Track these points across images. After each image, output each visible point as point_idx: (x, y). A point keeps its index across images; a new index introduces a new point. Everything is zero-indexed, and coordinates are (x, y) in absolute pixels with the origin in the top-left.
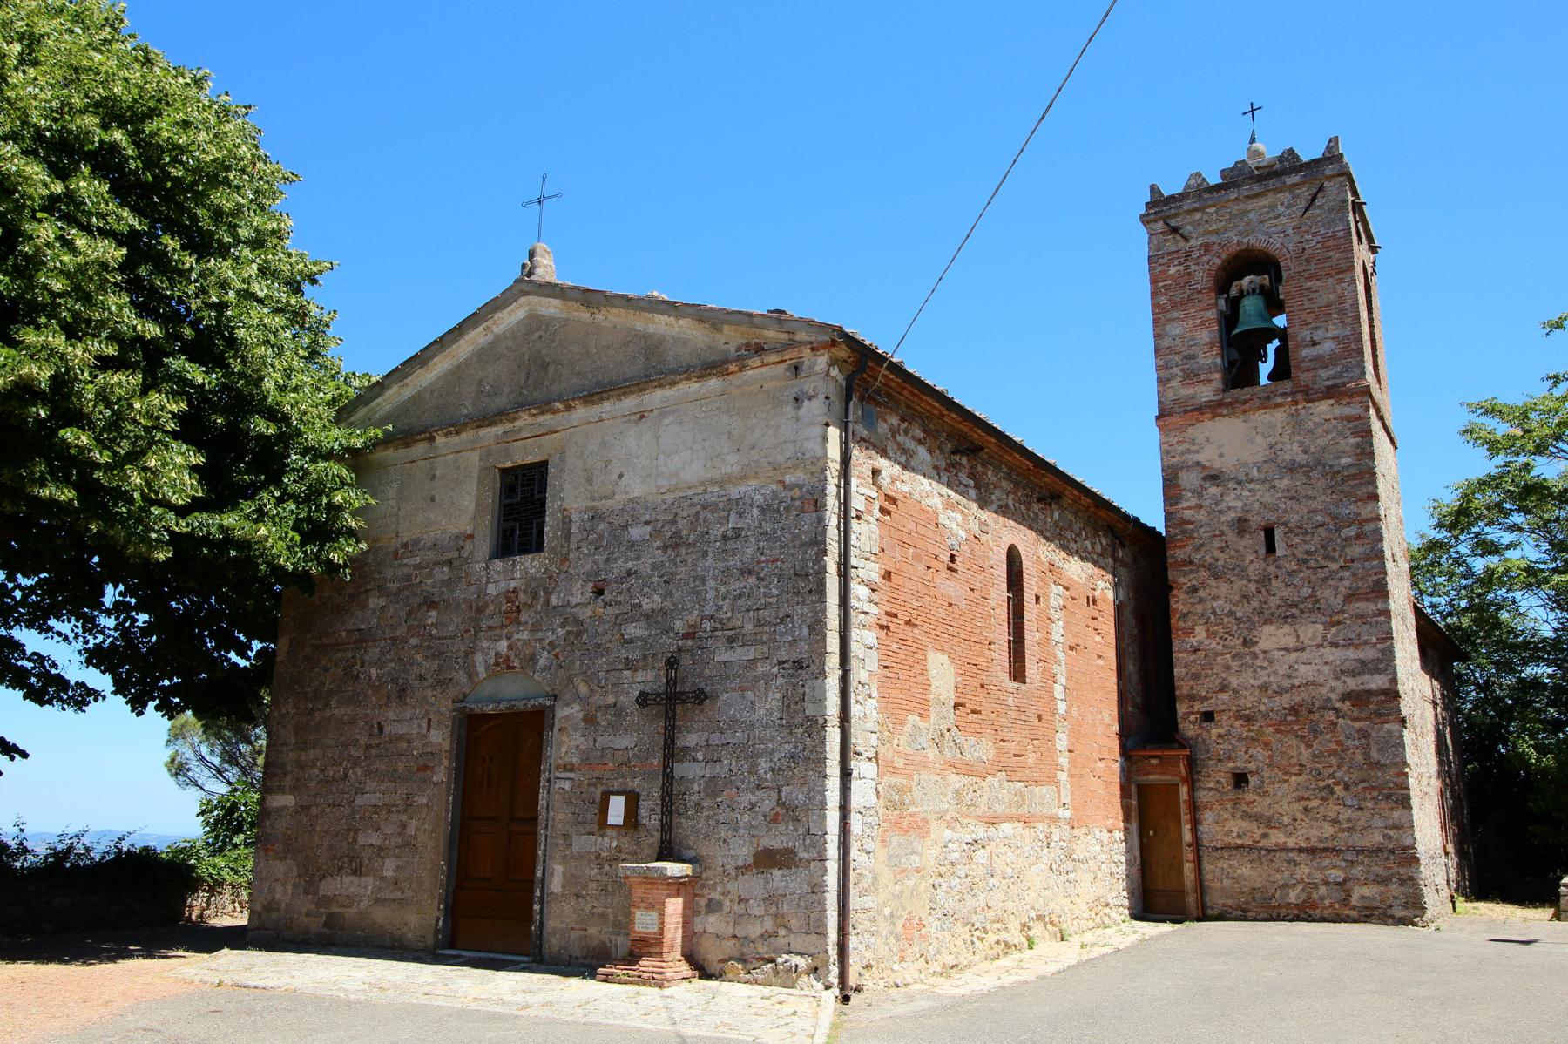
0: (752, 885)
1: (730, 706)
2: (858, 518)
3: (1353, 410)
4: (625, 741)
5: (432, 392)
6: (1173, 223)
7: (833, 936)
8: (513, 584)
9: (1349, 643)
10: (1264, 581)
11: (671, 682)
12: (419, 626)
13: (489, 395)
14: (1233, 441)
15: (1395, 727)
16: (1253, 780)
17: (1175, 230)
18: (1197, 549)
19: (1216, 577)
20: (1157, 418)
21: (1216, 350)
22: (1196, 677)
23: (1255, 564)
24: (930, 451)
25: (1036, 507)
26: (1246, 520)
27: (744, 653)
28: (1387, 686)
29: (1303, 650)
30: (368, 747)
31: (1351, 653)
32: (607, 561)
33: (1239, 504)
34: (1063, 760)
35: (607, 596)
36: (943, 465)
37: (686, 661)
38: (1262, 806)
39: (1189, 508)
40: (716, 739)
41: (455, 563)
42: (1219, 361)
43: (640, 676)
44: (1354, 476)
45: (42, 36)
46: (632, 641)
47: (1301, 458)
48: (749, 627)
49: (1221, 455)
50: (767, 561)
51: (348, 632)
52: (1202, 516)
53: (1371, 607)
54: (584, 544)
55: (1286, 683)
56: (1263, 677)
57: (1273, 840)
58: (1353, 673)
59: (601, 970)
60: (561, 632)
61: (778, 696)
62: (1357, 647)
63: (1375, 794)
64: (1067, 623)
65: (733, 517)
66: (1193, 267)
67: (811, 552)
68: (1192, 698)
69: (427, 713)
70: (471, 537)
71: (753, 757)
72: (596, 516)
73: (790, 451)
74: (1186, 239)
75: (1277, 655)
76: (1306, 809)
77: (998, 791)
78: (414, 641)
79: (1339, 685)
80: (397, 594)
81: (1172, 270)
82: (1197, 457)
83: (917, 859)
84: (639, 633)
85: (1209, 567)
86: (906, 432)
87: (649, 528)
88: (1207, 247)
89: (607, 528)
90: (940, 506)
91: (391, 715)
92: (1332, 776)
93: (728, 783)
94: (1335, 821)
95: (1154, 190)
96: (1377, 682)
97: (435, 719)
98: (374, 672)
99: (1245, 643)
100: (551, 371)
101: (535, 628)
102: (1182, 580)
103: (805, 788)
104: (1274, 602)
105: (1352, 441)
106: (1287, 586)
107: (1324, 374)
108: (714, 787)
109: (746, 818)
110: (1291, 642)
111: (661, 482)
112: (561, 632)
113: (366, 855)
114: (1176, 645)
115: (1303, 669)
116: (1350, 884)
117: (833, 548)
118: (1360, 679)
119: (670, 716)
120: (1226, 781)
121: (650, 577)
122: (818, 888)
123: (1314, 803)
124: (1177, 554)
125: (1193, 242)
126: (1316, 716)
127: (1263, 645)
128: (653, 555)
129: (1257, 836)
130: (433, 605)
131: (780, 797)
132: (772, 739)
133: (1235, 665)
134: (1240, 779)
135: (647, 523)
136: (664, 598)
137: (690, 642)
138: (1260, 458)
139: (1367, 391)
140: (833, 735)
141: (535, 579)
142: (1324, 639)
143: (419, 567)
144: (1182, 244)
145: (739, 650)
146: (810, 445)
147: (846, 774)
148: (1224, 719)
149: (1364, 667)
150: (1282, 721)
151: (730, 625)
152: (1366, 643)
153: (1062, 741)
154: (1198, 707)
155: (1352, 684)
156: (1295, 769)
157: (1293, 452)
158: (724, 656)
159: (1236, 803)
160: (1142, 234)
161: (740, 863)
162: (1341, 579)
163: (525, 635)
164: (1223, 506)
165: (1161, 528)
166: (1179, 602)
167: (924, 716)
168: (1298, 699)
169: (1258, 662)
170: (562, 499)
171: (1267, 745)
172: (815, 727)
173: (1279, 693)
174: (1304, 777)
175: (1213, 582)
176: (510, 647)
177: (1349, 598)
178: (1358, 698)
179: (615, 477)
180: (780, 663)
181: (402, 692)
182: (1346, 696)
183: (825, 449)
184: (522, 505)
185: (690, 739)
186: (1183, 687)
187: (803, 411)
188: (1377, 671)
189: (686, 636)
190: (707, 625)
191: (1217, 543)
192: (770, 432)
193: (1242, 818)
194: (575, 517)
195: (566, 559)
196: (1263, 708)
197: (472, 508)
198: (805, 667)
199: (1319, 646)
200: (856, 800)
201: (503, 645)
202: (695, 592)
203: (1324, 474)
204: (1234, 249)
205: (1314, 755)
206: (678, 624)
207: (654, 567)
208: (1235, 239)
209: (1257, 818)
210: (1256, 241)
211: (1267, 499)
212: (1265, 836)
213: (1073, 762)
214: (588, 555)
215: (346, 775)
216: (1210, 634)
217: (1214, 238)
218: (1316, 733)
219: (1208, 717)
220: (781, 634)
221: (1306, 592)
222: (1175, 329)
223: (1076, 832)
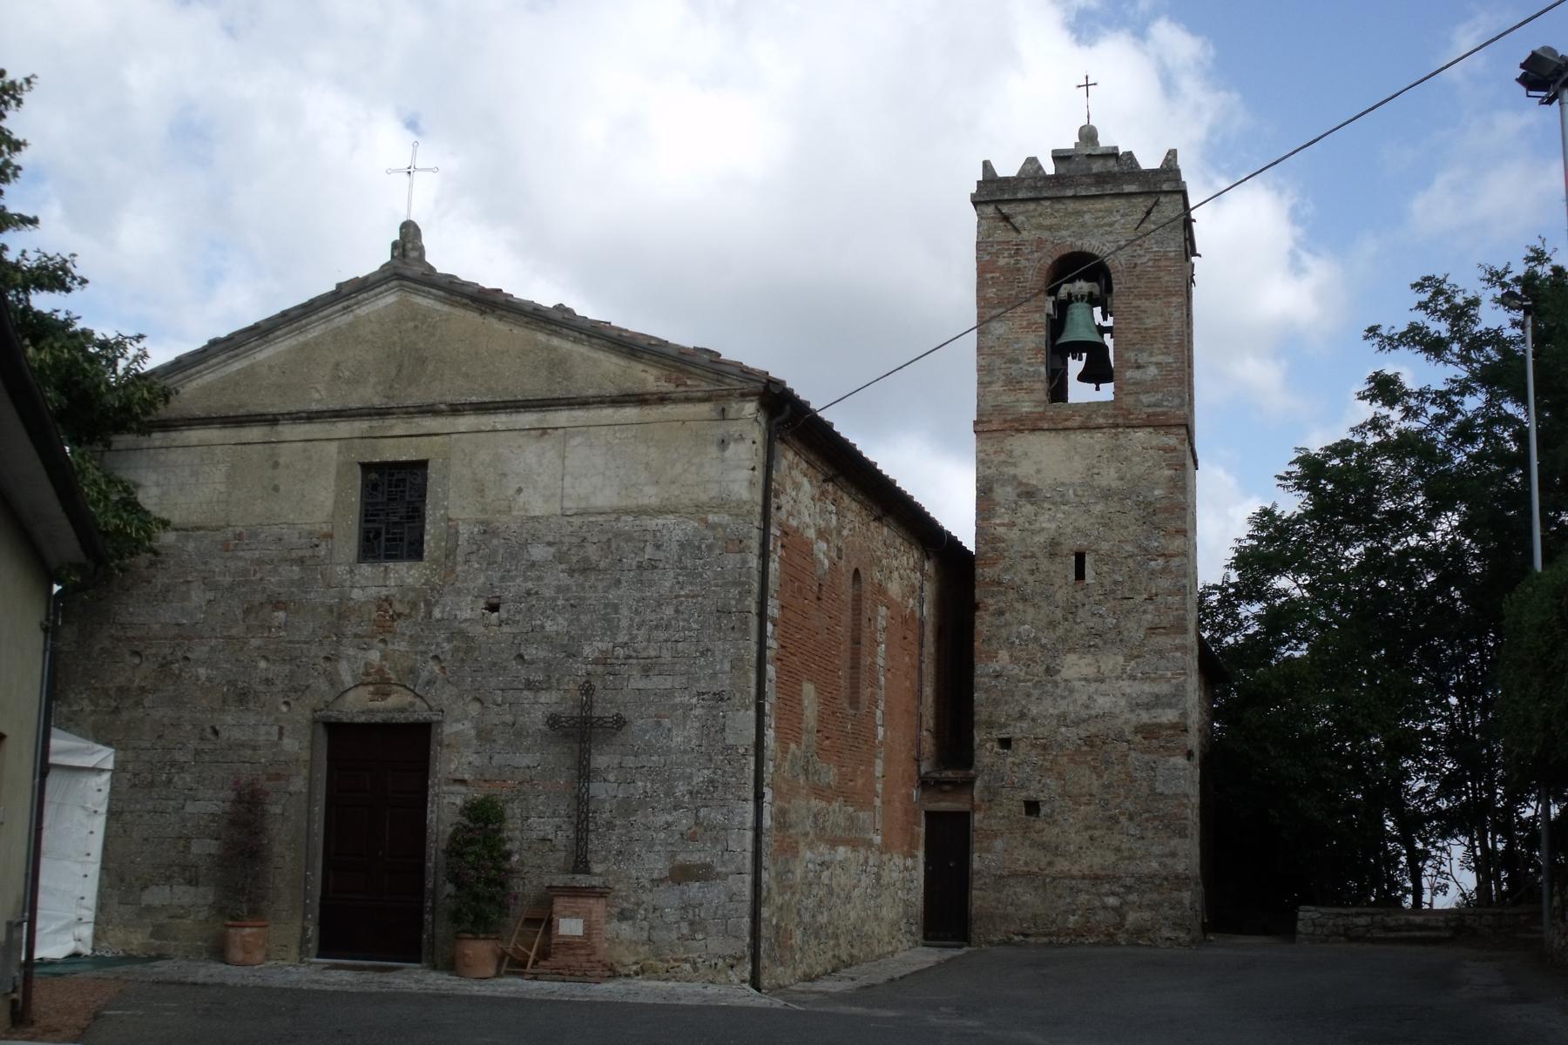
0: (668, 899)
3: (1172, 441)
4: (524, 760)
5: (271, 368)
6: (1005, 209)
8: (384, 592)
9: (1146, 677)
10: (1072, 610)
12: (262, 626)
13: (348, 382)
14: (1046, 458)
16: (1044, 810)
17: (1006, 218)
18: (1006, 570)
19: (1024, 600)
20: (976, 423)
21: (1041, 357)
22: (996, 703)
23: (1063, 592)
25: (873, 525)
26: (1058, 544)
27: (658, 682)
28: (1176, 720)
29: (1102, 681)
30: (197, 752)
31: (1147, 687)
32: (502, 579)
33: (1053, 526)
35: (503, 613)
38: (1051, 834)
40: (630, 762)
41: (309, 562)
42: (1043, 369)
43: (544, 697)
44: (1166, 510)
45: (1463, 895)
46: (532, 662)
47: (1115, 484)
48: (667, 656)
49: (1038, 471)
50: (687, 596)
51: (163, 625)
52: (1014, 534)
54: (473, 558)
55: (1084, 714)
56: (1063, 706)
57: (1058, 867)
58: (1148, 707)
61: (697, 725)
62: (1153, 680)
63: (1156, 823)
65: (649, 549)
66: (1023, 263)
68: (990, 725)
69: (277, 720)
70: (329, 536)
72: (488, 531)
73: (713, 490)
74: (1017, 230)
75: (1078, 684)
76: (1091, 838)
78: (255, 642)
79: (1133, 718)
80: (231, 588)
81: (1002, 262)
82: (1011, 471)
84: (542, 654)
85: (1017, 589)
87: (552, 550)
88: (1040, 243)
89: (499, 543)
91: (229, 719)
92: (1118, 806)
93: (642, 804)
94: (1118, 850)
97: (288, 728)
98: (202, 671)
99: (1050, 671)
100: (430, 368)
101: (414, 640)
102: (991, 601)
103: (725, 810)
104: (1081, 629)
105: (1168, 473)
107: (1145, 399)
108: (627, 808)
109: (662, 835)
110: (1090, 672)
111: (567, 504)
114: (980, 669)
115: (1101, 700)
116: (1125, 908)
118: (1154, 712)
120: (1018, 809)
121: (555, 599)
123: (1097, 833)
124: (983, 573)
125: (1025, 234)
126: (1107, 748)
127: (1065, 673)
128: (557, 576)
129: (1043, 865)
130: (278, 605)
131: (697, 817)
132: (691, 765)
133: (1036, 693)
134: (1032, 807)
135: (550, 544)
136: (571, 623)
137: (600, 669)
138: (1077, 479)
141: (413, 589)
142: (1124, 671)
143: (260, 562)
144: (1014, 234)
145: (655, 679)
148: (1022, 748)
149: (1157, 702)
150: (1078, 750)
151: (645, 654)
152: (1162, 677)
153: (879, 769)
154: (996, 734)
155: (1145, 717)
156: (1084, 799)
157: (1109, 477)
158: (638, 683)
159: (1026, 829)
160: (971, 216)
161: (655, 876)
162: (1145, 612)
163: (403, 646)
164: (1037, 526)
165: (969, 543)
166: (984, 623)
168: (1093, 730)
169: (1059, 691)
170: (446, 508)
171: (1060, 776)
173: (1076, 724)
174: (1092, 807)
175: (1019, 606)
176: (384, 657)
177: (1153, 629)
179: (511, 492)
180: (699, 694)
184: (393, 506)
185: (600, 760)
186: (981, 713)
187: (729, 453)
188: (1170, 706)
189: (596, 662)
190: (620, 652)
191: (1027, 564)
192: (693, 469)
193: (1031, 846)
194: (462, 529)
195: (453, 571)
196: (1059, 738)
197: (329, 503)
199: (1117, 678)
201: (374, 656)
202: (605, 618)
203: (1138, 504)
206: (587, 650)
207: (559, 589)
208: (1071, 241)
209: (1043, 846)
210: (1092, 244)
211: (1081, 523)
212: (1050, 864)
214: (480, 569)
215: (170, 781)
216: (1014, 659)
217: (1045, 235)
218: (1108, 763)
219: (1006, 743)
220: (701, 668)
221: (1111, 621)
222: (998, 328)
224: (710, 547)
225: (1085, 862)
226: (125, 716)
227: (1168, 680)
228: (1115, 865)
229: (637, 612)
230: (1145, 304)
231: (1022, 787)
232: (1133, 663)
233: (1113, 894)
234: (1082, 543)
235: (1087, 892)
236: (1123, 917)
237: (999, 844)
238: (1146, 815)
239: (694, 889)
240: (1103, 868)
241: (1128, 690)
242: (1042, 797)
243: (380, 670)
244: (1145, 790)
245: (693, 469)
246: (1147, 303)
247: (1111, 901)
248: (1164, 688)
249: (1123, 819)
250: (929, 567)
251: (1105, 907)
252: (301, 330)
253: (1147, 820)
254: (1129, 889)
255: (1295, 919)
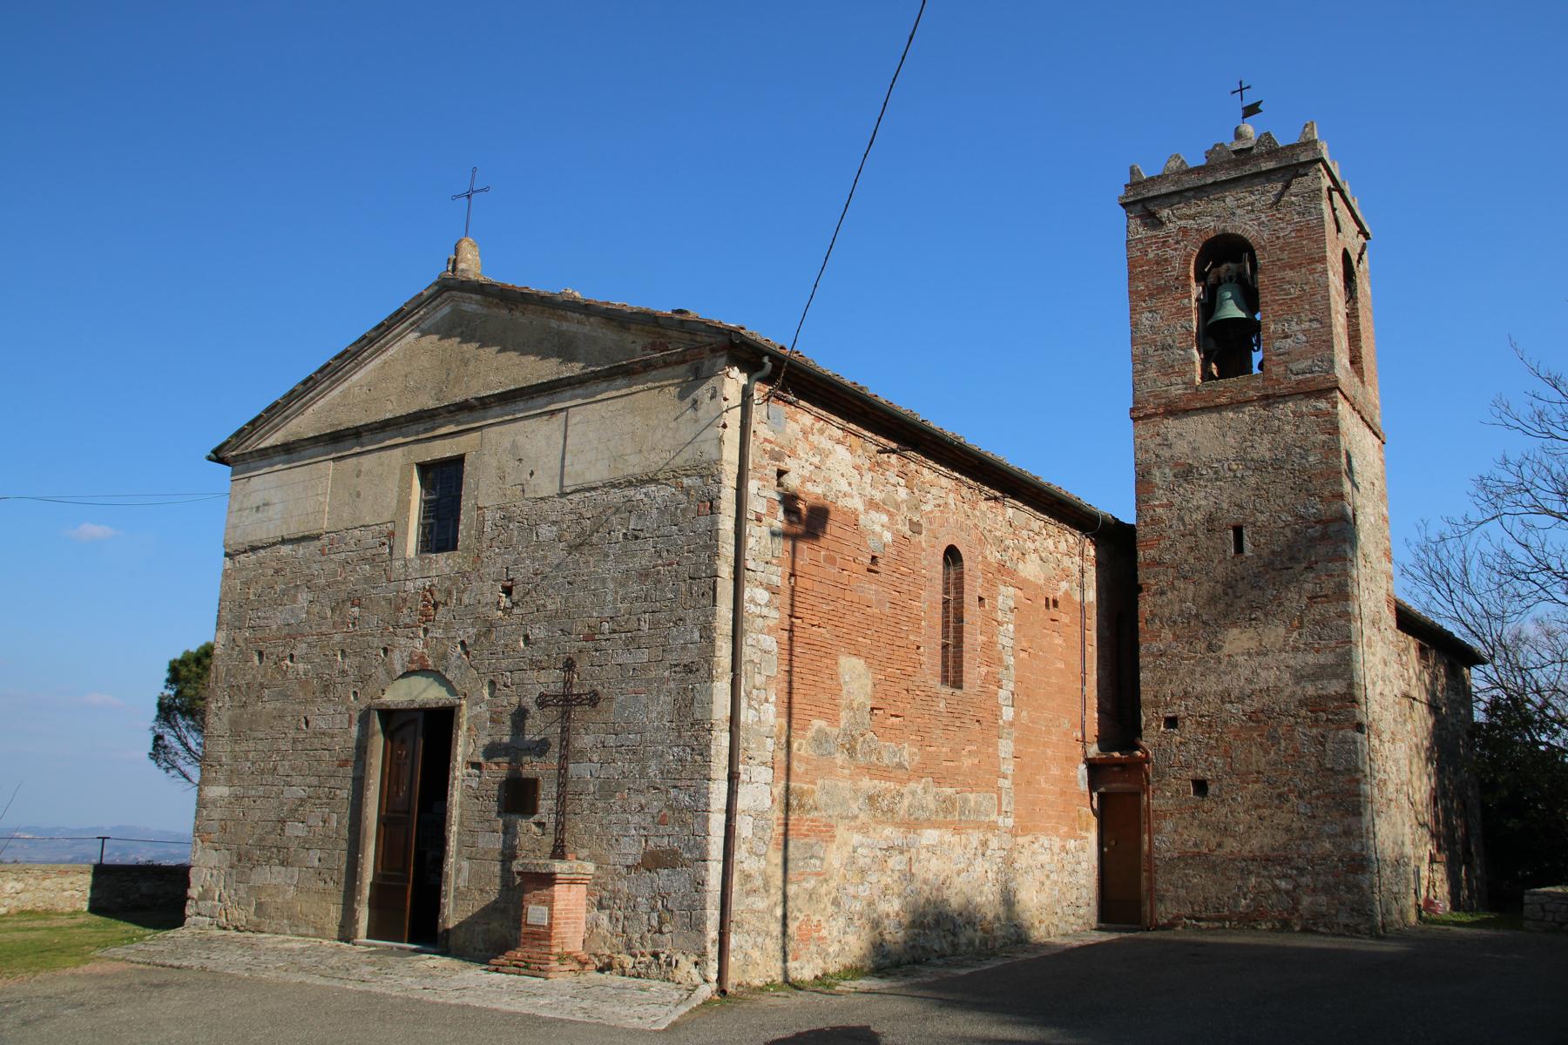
1: (624, 708)
2: (759, 520)
7: (713, 933)
11: (568, 683)
15: (1350, 733)
16: (1212, 789)
24: (850, 449)
31: (1311, 658)
34: (1008, 767)
36: (867, 464)
37: (582, 665)
39: (1161, 506)
53: (1332, 610)
59: (493, 961)
60: (471, 631)
64: (1018, 628)
67: (704, 556)
71: (643, 762)
75: (1241, 659)
77: (920, 794)
83: (818, 863)
86: (821, 431)
90: (861, 508)
94: (1288, 830)
95: (1133, 171)
96: (1335, 687)
99: (1210, 648)
101: (447, 627)
105: (1324, 437)
106: (1253, 587)
108: (607, 789)
110: (1253, 645)
112: (471, 631)
113: (293, 846)
117: (727, 549)
119: (565, 716)
122: (699, 884)
127: (1227, 649)
129: (1213, 844)
134: (1201, 786)
135: (554, 523)
137: (590, 644)
139: (1328, 390)
140: (721, 740)
142: (1286, 643)
146: (706, 447)
147: (733, 778)
149: (1319, 673)
153: (1006, 747)
155: (1310, 690)
157: (1263, 449)
166: (1145, 606)
167: (833, 720)
168: (1256, 705)
170: (476, 498)
172: (703, 727)
173: (1240, 700)
175: (1180, 584)
178: (1316, 705)
181: (326, 689)
182: (1303, 703)
183: (720, 451)
185: (584, 741)
186: (1146, 694)
188: (1336, 676)
198: (696, 670)
200: (742, 803)
204: (1212, 234)
205: (1268, 763)
212: (1219, 845)
213: (1020, 768)
219: (1172, 722)
223: (1020, 840)
224: (684, 511)
225: (1255, 843)
226: (250, 710)
227: (1333, 650)
228: (1285, 846)
229: (622, 585)
230: (1289, 274)
231: (1188, 766)
232: (1295, 634)
233: (1285, 876)
234: (1235, 516)
235: (1258, 875)
236: (1297, 901)
237: (1168, 825)
238: (1315, 793)
239: (662, 877)
240: (1273, 849)
241: (1292, 663)
242: (1208, 775)
243: (422, 657)
244: (1312, 767)
245: (670, 434)
246: (1291, 273)
247: (1283, 884)
248: (1323, 658)
249: (1292, 797)
250: (1091, 551)
251: (1277, 890)
252: (382, 350)
253: (1318, 798)
254: (1301, 871)
255: (1521, 904)
